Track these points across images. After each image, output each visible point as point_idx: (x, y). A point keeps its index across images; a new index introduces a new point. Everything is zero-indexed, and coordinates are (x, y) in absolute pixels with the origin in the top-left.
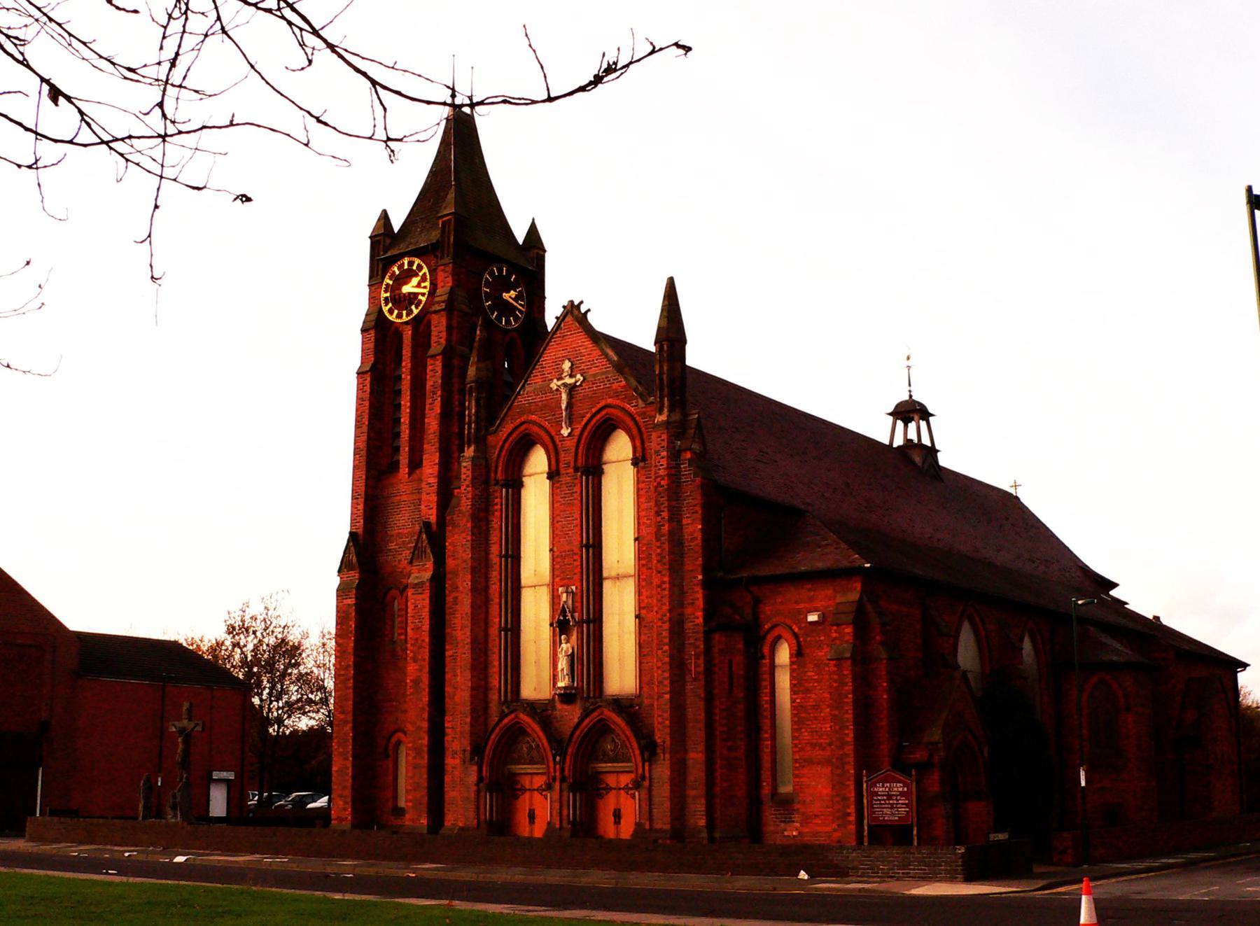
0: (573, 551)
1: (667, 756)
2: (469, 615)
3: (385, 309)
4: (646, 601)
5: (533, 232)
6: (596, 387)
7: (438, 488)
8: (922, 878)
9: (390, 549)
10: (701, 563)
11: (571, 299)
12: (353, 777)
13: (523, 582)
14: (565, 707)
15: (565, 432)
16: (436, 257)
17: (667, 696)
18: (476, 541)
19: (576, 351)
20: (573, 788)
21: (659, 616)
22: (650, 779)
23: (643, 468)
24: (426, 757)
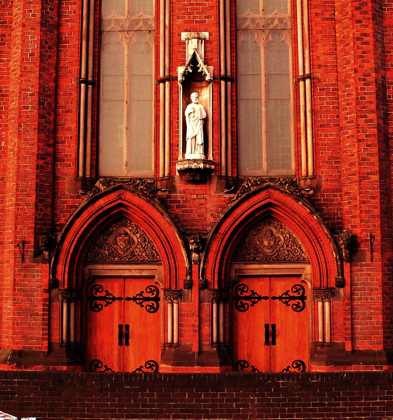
1: (377, 255)
2: (37, 55)
14: (191, 187)
17: (376, 177)
21: (360, 75)
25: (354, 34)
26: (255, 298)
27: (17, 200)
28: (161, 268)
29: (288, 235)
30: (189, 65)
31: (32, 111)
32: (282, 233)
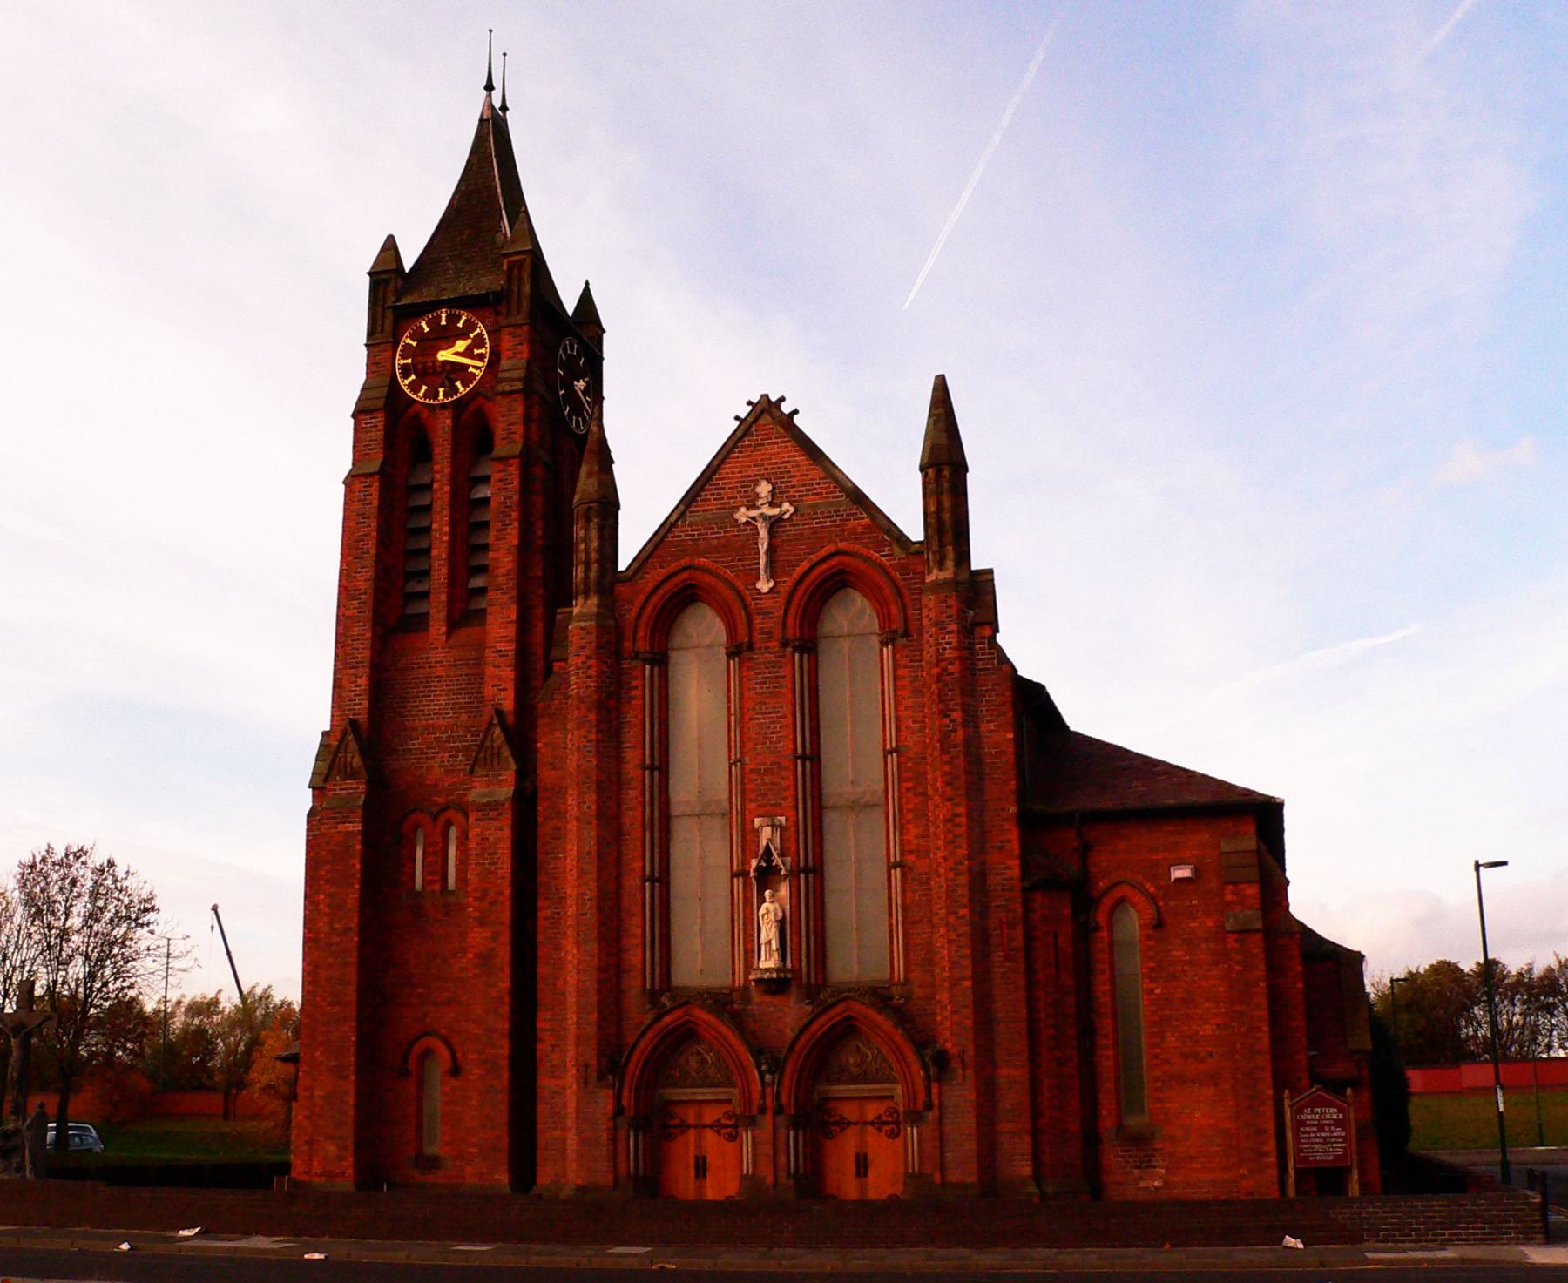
0: (779, 763)
1: (970, 1073)
2: (594, 853)
3: (404, 383)
4: (915, 841)
5: (586, 299)
6: (817, 523)
7: (516, 660)
8: (1480, 1240)
9: (411, 750)
10: (1014, 787)
11: (765, 392)
12: (357, 1106)
13: (676, 810)
14: (768, 999)
15: (764, 586)
16: (498, 313)
17: (968, 983)
18: (603, 741)
19: (779, 468)
20: (795, 1124)
22: (941, 1106)
23: (904, 646)
24: (506, 1075)
25: (944, 815)
26: (877, 1123)
27: (578, 1018)
28: (736, 1091)
29: (876, 1051)
30: (762, 858)
31: (591, 917)
32: (870, 1049)
